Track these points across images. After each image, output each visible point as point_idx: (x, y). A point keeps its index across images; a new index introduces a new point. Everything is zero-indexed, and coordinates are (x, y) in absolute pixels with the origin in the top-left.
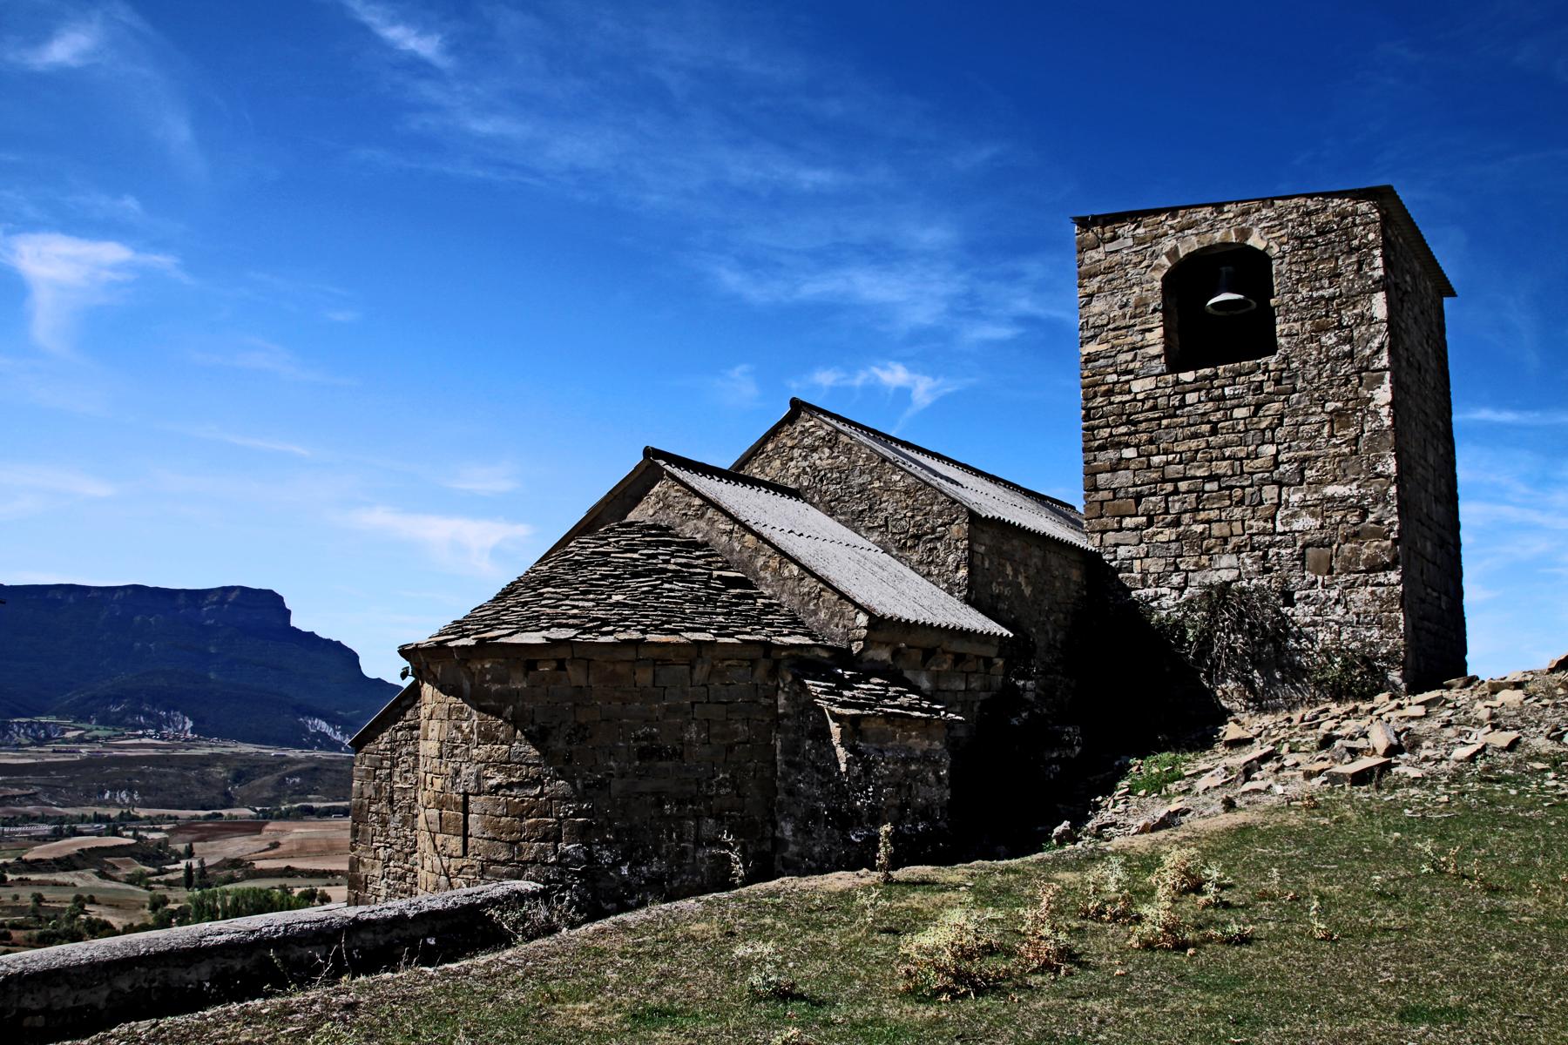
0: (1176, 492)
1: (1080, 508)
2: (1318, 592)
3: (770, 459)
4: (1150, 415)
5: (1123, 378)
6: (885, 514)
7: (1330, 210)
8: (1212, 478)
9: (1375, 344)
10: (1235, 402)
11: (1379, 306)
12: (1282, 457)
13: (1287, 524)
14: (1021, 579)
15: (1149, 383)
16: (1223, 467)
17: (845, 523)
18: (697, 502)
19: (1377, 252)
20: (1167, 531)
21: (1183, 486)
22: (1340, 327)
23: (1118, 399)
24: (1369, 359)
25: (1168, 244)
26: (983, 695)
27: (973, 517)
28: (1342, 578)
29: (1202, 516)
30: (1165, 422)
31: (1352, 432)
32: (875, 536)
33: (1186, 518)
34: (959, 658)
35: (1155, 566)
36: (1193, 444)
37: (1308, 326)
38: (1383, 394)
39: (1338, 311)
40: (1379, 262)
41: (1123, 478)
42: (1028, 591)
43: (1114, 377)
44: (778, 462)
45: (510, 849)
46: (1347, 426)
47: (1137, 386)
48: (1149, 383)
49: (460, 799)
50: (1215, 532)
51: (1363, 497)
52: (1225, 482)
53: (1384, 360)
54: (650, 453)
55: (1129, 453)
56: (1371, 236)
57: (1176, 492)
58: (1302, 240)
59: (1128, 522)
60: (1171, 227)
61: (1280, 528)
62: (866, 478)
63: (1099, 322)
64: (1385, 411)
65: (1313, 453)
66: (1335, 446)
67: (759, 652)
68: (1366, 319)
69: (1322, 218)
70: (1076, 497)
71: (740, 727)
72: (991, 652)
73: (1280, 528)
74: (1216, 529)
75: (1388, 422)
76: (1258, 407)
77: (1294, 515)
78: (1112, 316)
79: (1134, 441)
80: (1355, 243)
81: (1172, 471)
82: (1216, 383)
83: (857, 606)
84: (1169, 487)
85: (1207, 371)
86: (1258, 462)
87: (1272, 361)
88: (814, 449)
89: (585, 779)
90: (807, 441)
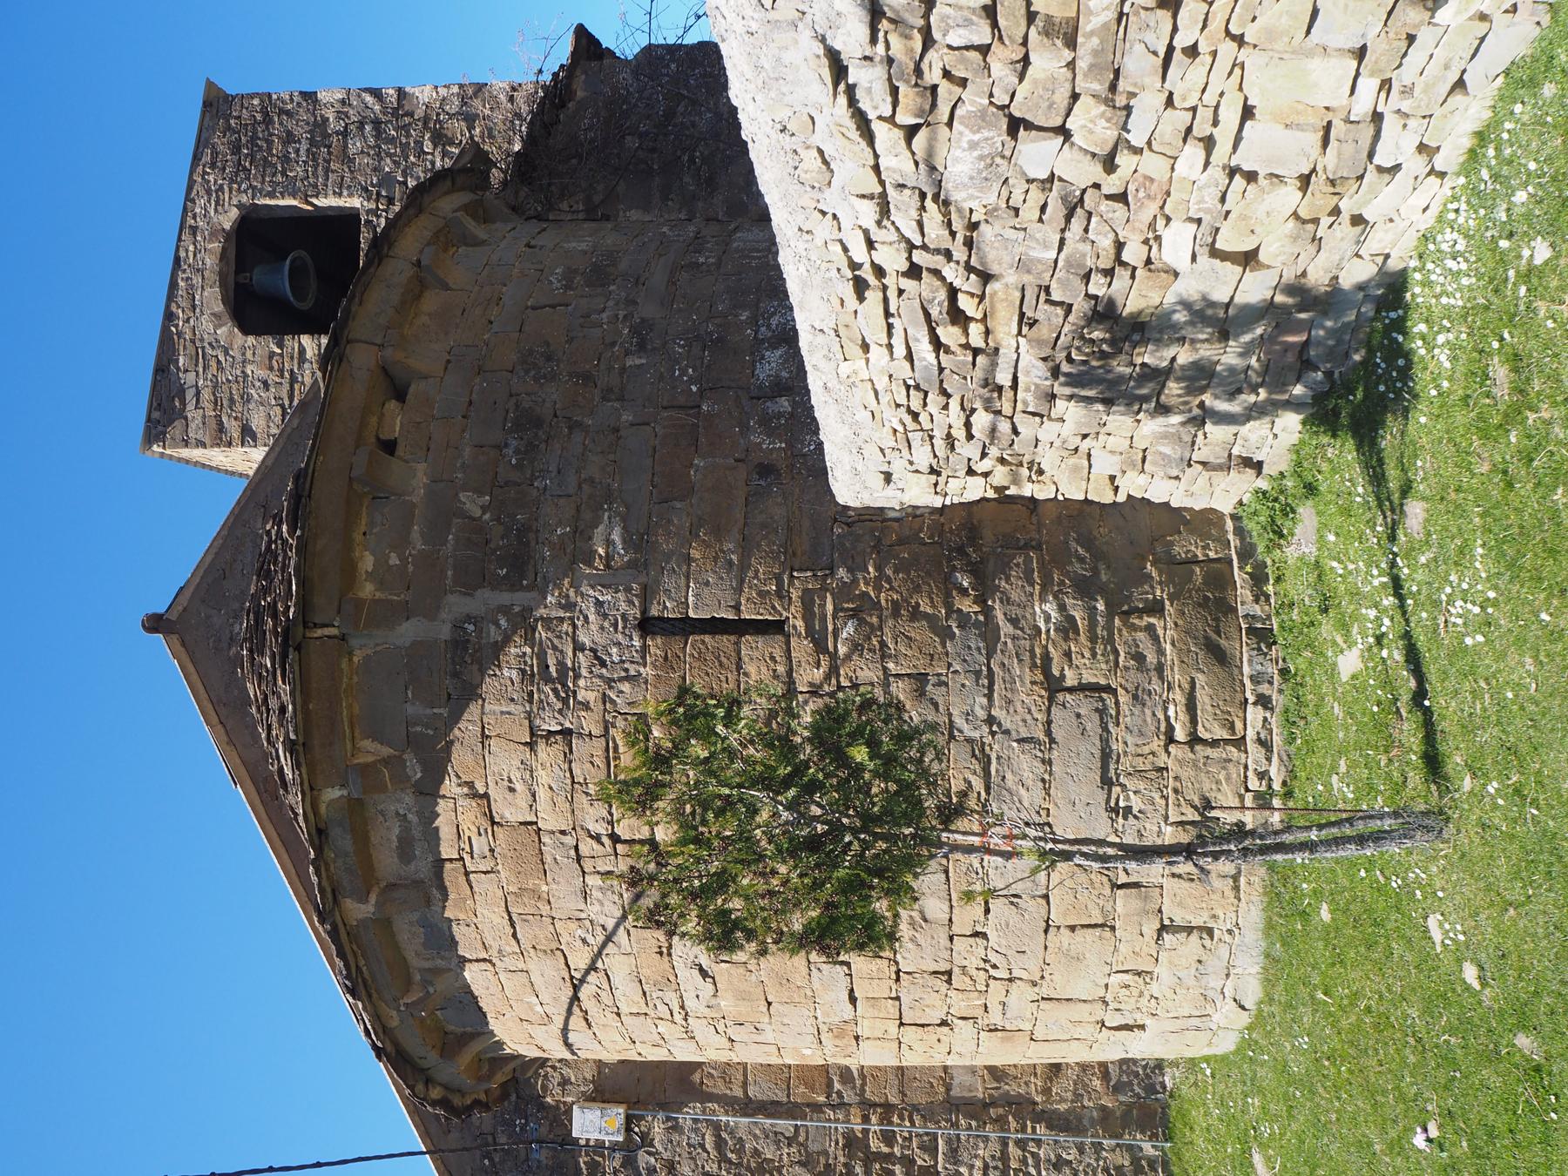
25: (206, 325)
78: (273, 402)
89: (627, 353)
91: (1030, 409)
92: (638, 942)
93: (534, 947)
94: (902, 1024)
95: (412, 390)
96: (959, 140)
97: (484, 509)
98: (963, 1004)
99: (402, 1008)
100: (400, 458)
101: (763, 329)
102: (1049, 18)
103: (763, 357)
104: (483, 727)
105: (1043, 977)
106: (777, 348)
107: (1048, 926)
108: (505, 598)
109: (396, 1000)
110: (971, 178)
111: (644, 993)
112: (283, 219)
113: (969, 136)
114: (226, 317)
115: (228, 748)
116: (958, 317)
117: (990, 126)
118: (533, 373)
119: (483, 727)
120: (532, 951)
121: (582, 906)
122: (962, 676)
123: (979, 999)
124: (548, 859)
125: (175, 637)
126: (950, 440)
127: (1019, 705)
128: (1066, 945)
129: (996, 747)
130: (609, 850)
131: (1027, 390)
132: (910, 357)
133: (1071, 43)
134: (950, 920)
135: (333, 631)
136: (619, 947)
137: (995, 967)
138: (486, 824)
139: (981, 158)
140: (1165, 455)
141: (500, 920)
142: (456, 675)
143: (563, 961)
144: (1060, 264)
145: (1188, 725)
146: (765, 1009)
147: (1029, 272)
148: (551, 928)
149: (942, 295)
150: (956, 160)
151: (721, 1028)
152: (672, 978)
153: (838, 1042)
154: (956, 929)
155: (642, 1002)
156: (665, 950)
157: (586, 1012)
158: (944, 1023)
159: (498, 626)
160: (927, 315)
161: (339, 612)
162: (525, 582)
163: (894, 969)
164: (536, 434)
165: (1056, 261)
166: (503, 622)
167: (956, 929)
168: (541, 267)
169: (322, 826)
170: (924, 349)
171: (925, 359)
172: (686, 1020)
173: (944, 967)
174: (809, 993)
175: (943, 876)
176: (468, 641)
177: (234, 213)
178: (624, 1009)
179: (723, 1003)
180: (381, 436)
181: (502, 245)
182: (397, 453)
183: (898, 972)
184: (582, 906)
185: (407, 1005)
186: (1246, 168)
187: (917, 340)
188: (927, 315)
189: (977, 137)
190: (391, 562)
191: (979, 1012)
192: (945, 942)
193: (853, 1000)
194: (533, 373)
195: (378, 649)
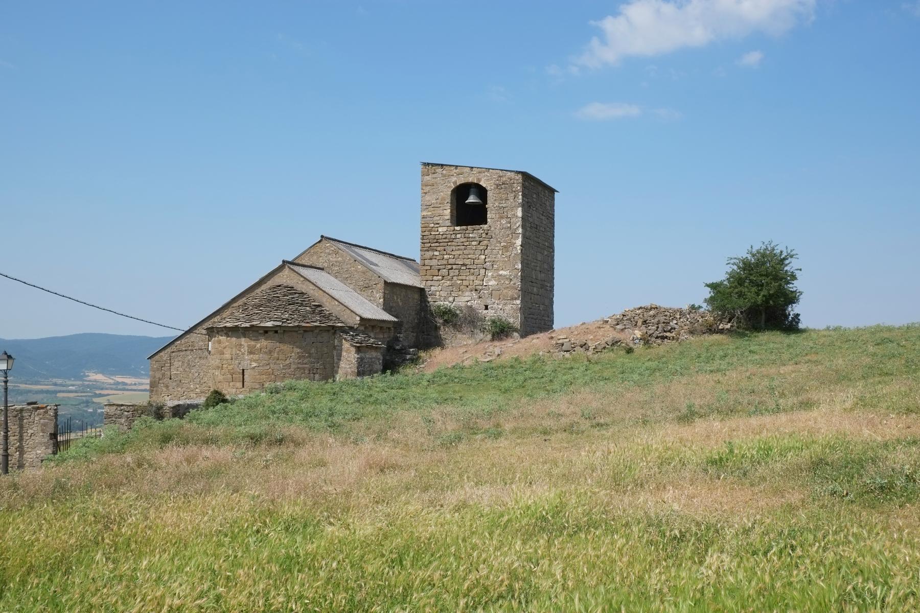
0: (452, 269)
1: (418, 261)
2: (495, 306)
3: (312, 255)
4: (444, 240)
5: (436, 226)
6: (355, 279)
7: (507, 177)
8: (464, 265)
9: (518, 225)
10: (473, 239)
11: (519, 212)
12: (486, 260)
13: (487, 283)
14: (399, 300)
15: (445, 229)
16: (467, 262)
17: (341, 281)
18: (302, 279)
19: (520, 194)
20: (448, 282)
21: (454, 267)
22: (507, 218)
23: (433, 233)
24: (515, 230)
25: (454, 179)
26: (388, 339)
27: (385, 282)
28: (503, 302)
29: (460, 278)
30: (449, 244)
31: (508, 254)
32: (352, 286)
33: (455, 278)
34: (381, 328)
35: (443, 294)
36: (458, 252)
37: (497, 216)
38: (519, 242)
39: (507, 212)
40: (520, 197)
41: (434, 262)
42: (401, 304)
43: (432, 225)
44: (315, 257)
45: (260, 385)
46: (507, 252)
47: (440, 229)
48: (445, 229)
49: (241, 371)
50: (464, 284)
51: (511, 275)
52: (468, 267)
53: (520, 230)
54: (284, 261)
55: (436, 253)
56: (519, 188)
57: (452, 269)
58: (497, 185)
59: (435, 278)
60: (455, 173)
61: (485, 284)
62: (349, 266)
63: (428, 204)
64: (519, 248)
65: (496, 260)
66: (503, 258)
67: (331, 328)
68: (515, 216)
69: (504, 179)
70: (414, 252)
71: (325, 349)
72: (391, 326)
73: (485, 284)
74: (465, 283)
75: (519, 251)
76: (480, 242)
77: (489, 280)
79: (439, 249)
80: (514, 189)
81: (451, 261)
82: (467, 232)
83: (356, 314)
84: (450, 267)
85: (464, 227)
86: (479, 261)
87: (485, 227)
88: (329, 254)
90: (327, 251)
177: (484, 186)
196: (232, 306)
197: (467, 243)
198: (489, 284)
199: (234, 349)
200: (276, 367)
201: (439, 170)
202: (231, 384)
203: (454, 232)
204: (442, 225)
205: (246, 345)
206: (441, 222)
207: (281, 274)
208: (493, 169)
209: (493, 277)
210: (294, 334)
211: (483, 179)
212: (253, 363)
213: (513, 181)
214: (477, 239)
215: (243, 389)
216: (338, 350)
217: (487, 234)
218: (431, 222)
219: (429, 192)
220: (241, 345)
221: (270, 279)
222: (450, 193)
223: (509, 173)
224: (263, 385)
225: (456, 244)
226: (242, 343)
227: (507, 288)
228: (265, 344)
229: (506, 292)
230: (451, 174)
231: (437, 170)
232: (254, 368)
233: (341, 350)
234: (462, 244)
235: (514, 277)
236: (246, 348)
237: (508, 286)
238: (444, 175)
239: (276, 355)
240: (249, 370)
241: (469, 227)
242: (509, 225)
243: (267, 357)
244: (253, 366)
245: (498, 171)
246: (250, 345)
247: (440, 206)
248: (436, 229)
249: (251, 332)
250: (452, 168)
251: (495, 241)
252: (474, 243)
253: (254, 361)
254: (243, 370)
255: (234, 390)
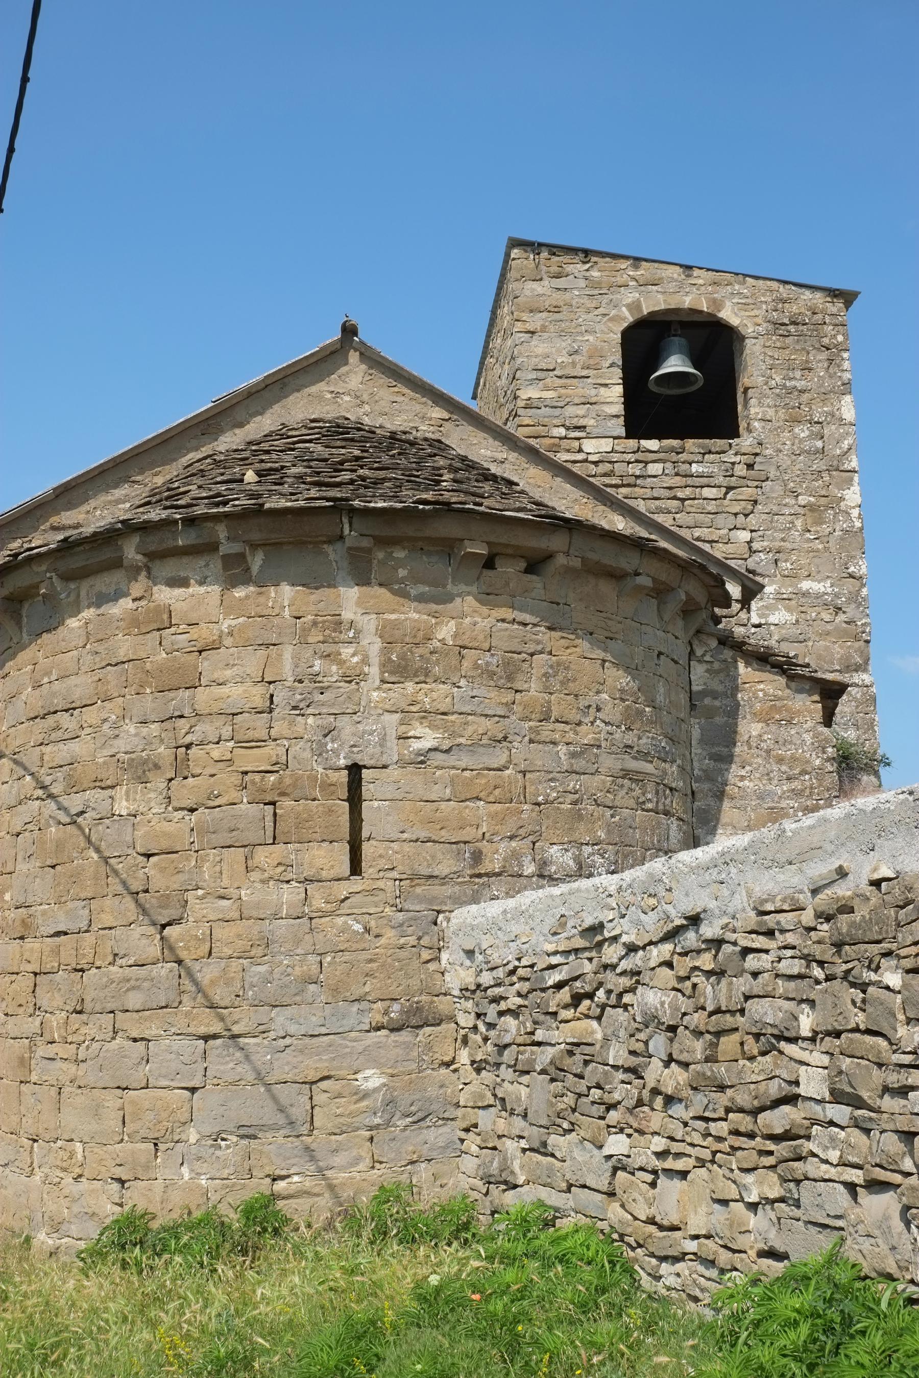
10: (704, 481)
25: (630, 296)
43: (562, 431)
47: (589, 446)
48: (606, 445)
51: (837, 596)
61: (755, 620)
65: (788, 545)
69: (795, 309)
85: (675, 443)
91: (520, 1056)
92: (105, 763)
93: (100, 680)
94: (36, 974)
95: (534, 577)
96: (666, 995)
97: (441, 640)
98: (55, 1024)
99: (48, 575)
100: (481, 573)
101: (590, 850)
102: (717, 1045)
103: (566, 850)
104: (275, 645)
105: (80, 1087)
106: (575, 861)
107: (124, 1089)
108: (375, 660)
109: (55, 570)
110: (646, 1004)
111: (61, 766)
112: (733, 365)
113: (667, 1000)
114: (638, 316)
115: (245, 393)
116: (577, 1000)
117: (672, 1014)
118: (550, 671)
119: (275, 645)
120: (96, 678)
121: (135, 720)
122: (321, 1014)
123: (59, 1036)
124: (171, 694)
125: (338, 346)
126: (496, 1000)
127: (300, 1059)
128: (107, 1104)
129: (265, 1042)
130: (180, 742)
131: (532, 1053)
132: (552, 967)
133: (707, 1060)
134: (127, 1011)
135: (346, 531)
136: (100, 748)
137: (88, 1048)
138: (199, 646)
139: (656, 1009)
140: (492, 1163)
141: (122, 655)
142: (315, 623)
143: (89, 702)
144: (606, 1068)
145: (286, 1193)
146: (48, 863)
147: (602, 1047)
148: (116, 694)
149: (588, 988)
150: (656, 994)
151: (29, 827)
152: (74, 789)
153: (17, 923)
154: (120, 1015)
155: (54, 765)
156: (98, 784)
157: (43, 718)
158: (36, 1007)
159: (353, 655)
160: (576, 979)
161: (361, 535)
162: (386, 675)
163: (86, 967)
164: (501, 678)
165: (607, 1065)
166: (355, 659)
167: (120, 1015)
168: (639, 668)
169: (196, 523)
170: (554, 978)
171: (550, 978)
172: (37, 799)
173: (88, 1006)
174: (63, 899)
175: (163, 1004)
176: (341, 632)
177: (734, 321)
178: (46, 749)
179: (53, 829)
180: (497, 558)
181: (660, 633)
182: (484, 570)
183: (82, 970)
184: (135, 720)
185: (51, 578)
186: (659, 1181)
187: (560, 973)
188: (576, 979)
189: (666, 1006)
190: (400, 570)
191: (47, 1037)
192: (110, 1007)
193: (58, 934)
194: (550, 671)
195: (334, 564)
196: (54, 520)
197: (688, 492)
198: (773, 619)
199: (288, 652)
200: (539, 757)
201: (577, 268)
202: (264, 856)
203: (639, 456)
204: (595, 432)
205: (369, 624)
206: (592, 422)
207: (322, 386)
208: (757, 278)
209: (780, 598)
210: (606, 588)
211: (728, 304)
212: (418, 729)
213: (820, 316)
214: (720, 480)
215: (357, 884)
216: (710, 714)
217: (750, 466)
218: (555, 422)
219: (544, 329)
220: (338, 625)
221: (270, 405)
222: (618, 337)
223: (807, 294)
224: (477, 857)
225: (648, 493)
226: (347, 615)
227: (828, 633)
228: (484, 624)
229: (827, 648)
230: (620, 280)
231: (569, 268)
232: (421, 760)
233: (733, 712)
234: (667, 493)
235: (849, 601)
236: (374, 646)
237: (829, 627)
238: (593, 284)
239: (534, 688)
240: (394, 772)
241: (690, 443)
242: (819, 444)
243: (494, 699)
244: (416, 745)
245: (775, 285)
246: (395, 624)
247: (585, 373)
248: (576, 444)
249: (400, 554)
250: (623, 264)
251: (779, 489)
252: (707, 492)
253: (425, 715)
254: (355, 770)
255: (289, 895)
